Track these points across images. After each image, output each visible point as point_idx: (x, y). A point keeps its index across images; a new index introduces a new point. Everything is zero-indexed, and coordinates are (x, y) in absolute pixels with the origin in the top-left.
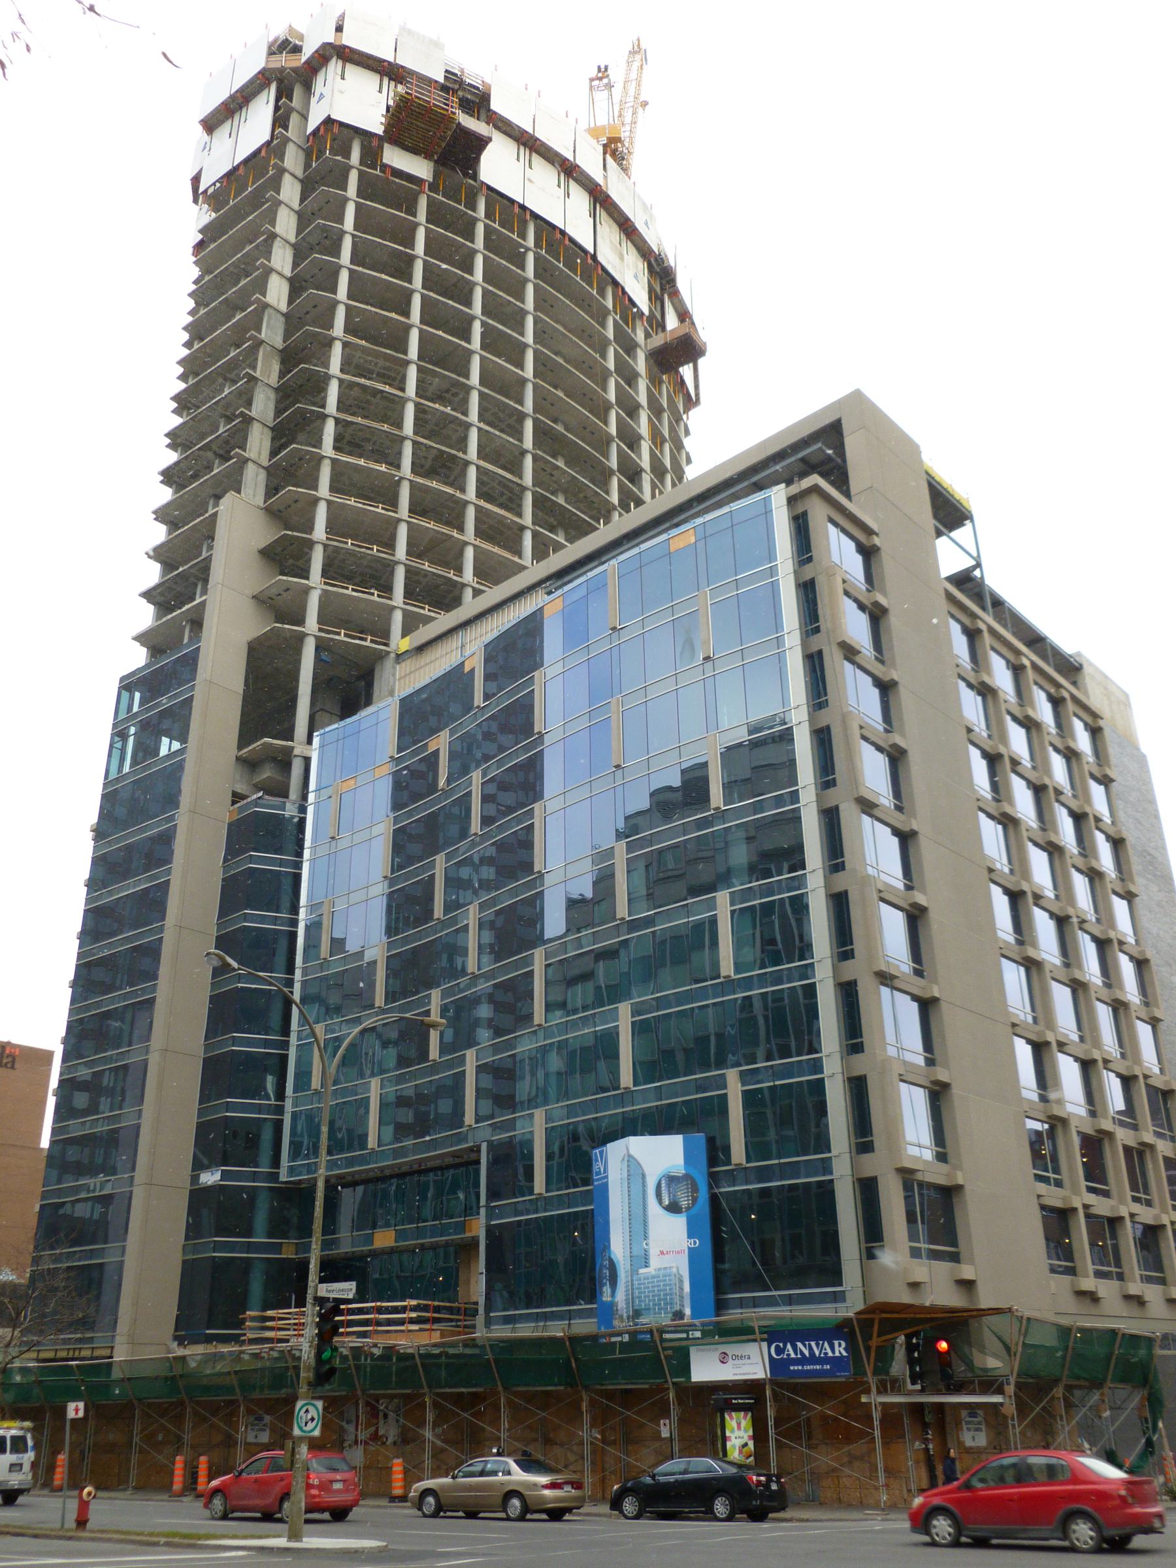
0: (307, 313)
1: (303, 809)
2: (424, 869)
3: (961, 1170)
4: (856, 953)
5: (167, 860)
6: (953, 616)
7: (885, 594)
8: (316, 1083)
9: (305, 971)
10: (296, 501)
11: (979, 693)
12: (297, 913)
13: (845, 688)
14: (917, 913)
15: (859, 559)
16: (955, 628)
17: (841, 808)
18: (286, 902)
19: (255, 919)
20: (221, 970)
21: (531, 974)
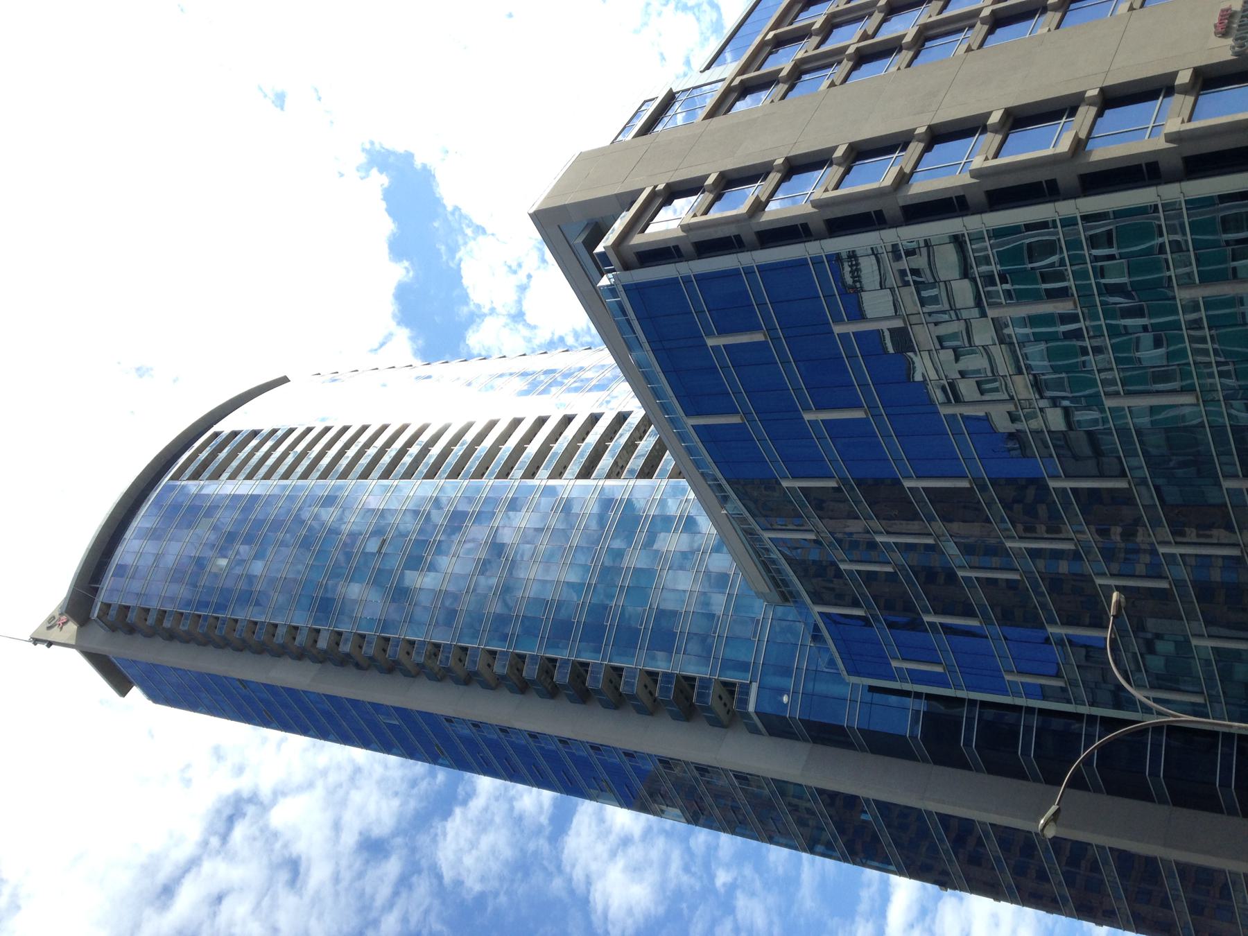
0: (725, 705)
1: (918, 695)
2: (853, 579)
3: (1085, 92)
4: (877, 208)
5: (1150, 862)
6: (729, 110)
7: (706, 177)
8: (1198, 699)
9: (958, 687)
10: (720, 697)
11: (799, 78)
12: (1021, 707)
13: (667, 230)
14: (1011, 120)
15: (678, 203)
16: (741, 106)
17: (902, 203)
18: (1010, 717)
19: (1026, 748)
20: (1077, 783)
21: (1074, 490)
